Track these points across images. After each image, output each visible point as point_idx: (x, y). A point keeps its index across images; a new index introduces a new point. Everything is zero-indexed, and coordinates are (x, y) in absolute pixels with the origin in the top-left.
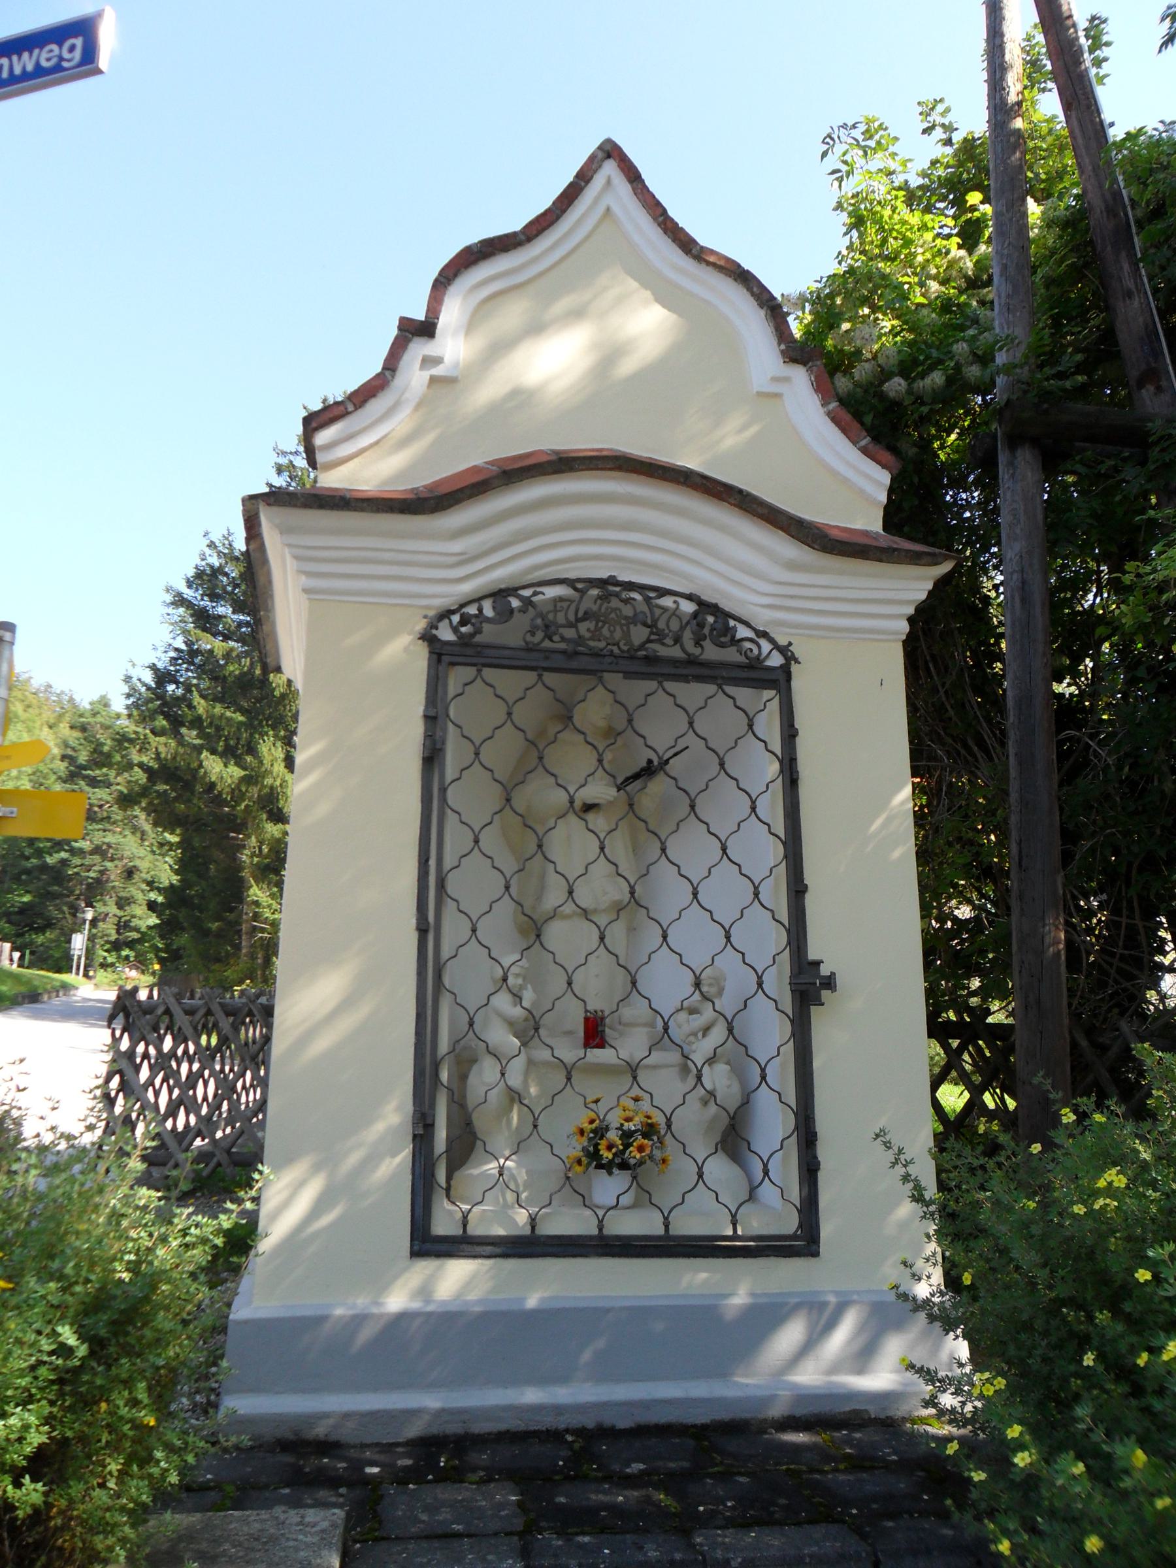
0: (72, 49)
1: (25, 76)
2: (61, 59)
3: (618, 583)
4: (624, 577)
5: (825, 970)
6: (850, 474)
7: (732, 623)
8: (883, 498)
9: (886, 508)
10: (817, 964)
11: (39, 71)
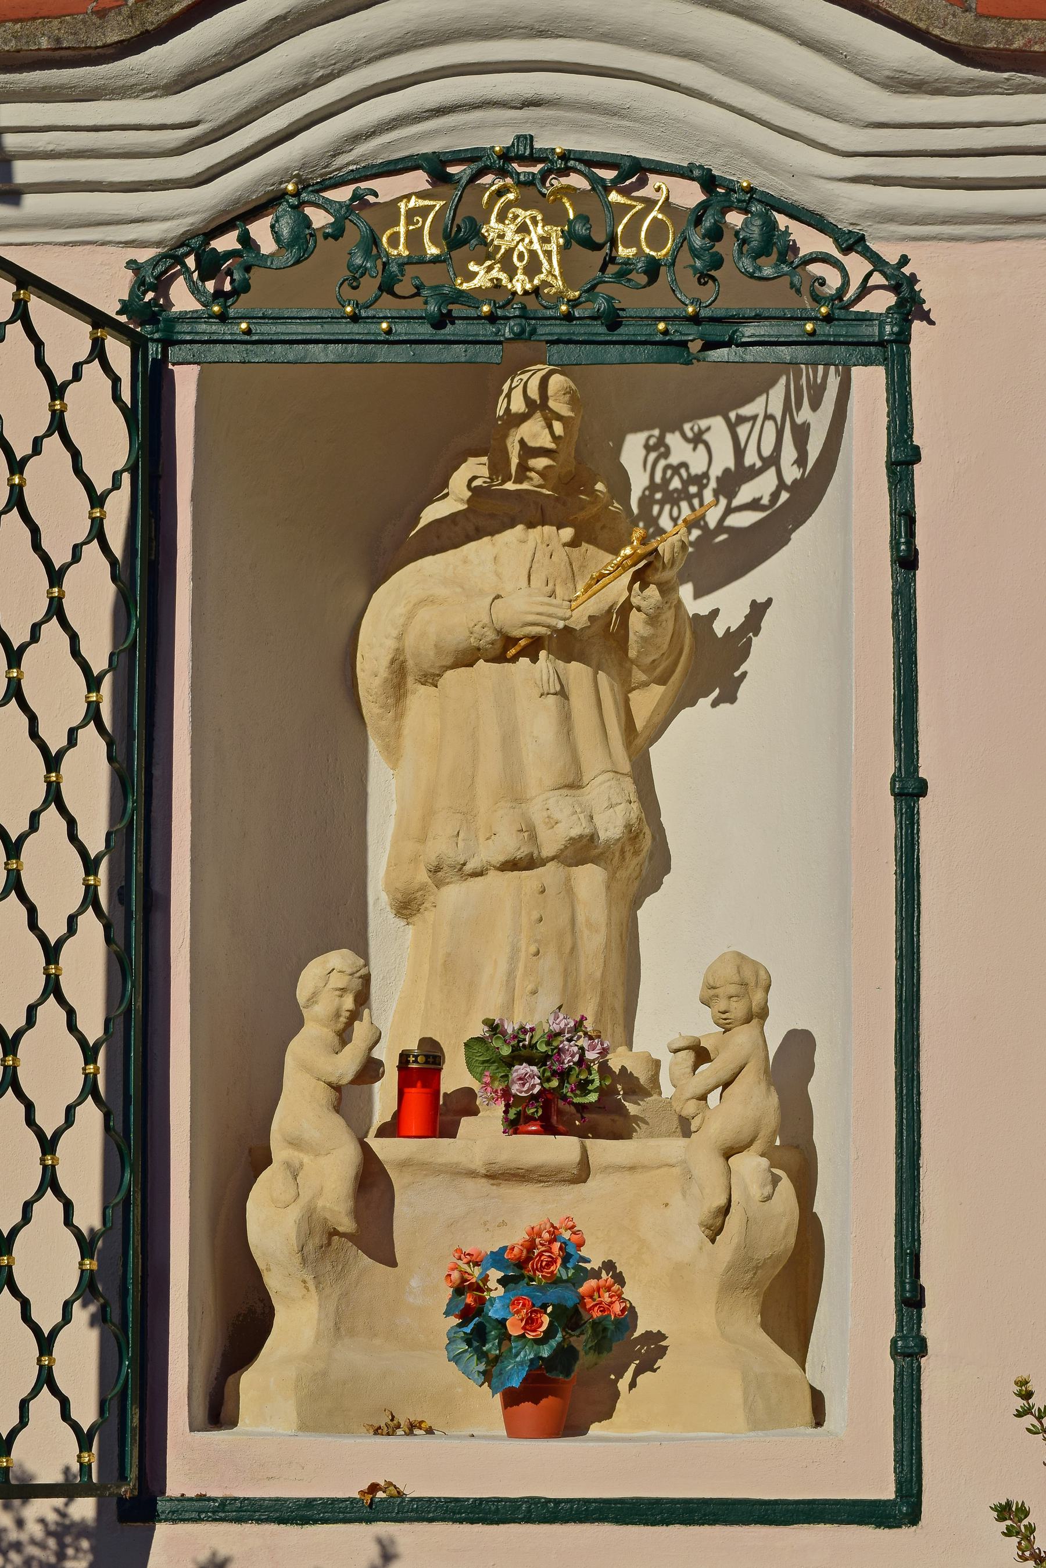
7: (782, 221)
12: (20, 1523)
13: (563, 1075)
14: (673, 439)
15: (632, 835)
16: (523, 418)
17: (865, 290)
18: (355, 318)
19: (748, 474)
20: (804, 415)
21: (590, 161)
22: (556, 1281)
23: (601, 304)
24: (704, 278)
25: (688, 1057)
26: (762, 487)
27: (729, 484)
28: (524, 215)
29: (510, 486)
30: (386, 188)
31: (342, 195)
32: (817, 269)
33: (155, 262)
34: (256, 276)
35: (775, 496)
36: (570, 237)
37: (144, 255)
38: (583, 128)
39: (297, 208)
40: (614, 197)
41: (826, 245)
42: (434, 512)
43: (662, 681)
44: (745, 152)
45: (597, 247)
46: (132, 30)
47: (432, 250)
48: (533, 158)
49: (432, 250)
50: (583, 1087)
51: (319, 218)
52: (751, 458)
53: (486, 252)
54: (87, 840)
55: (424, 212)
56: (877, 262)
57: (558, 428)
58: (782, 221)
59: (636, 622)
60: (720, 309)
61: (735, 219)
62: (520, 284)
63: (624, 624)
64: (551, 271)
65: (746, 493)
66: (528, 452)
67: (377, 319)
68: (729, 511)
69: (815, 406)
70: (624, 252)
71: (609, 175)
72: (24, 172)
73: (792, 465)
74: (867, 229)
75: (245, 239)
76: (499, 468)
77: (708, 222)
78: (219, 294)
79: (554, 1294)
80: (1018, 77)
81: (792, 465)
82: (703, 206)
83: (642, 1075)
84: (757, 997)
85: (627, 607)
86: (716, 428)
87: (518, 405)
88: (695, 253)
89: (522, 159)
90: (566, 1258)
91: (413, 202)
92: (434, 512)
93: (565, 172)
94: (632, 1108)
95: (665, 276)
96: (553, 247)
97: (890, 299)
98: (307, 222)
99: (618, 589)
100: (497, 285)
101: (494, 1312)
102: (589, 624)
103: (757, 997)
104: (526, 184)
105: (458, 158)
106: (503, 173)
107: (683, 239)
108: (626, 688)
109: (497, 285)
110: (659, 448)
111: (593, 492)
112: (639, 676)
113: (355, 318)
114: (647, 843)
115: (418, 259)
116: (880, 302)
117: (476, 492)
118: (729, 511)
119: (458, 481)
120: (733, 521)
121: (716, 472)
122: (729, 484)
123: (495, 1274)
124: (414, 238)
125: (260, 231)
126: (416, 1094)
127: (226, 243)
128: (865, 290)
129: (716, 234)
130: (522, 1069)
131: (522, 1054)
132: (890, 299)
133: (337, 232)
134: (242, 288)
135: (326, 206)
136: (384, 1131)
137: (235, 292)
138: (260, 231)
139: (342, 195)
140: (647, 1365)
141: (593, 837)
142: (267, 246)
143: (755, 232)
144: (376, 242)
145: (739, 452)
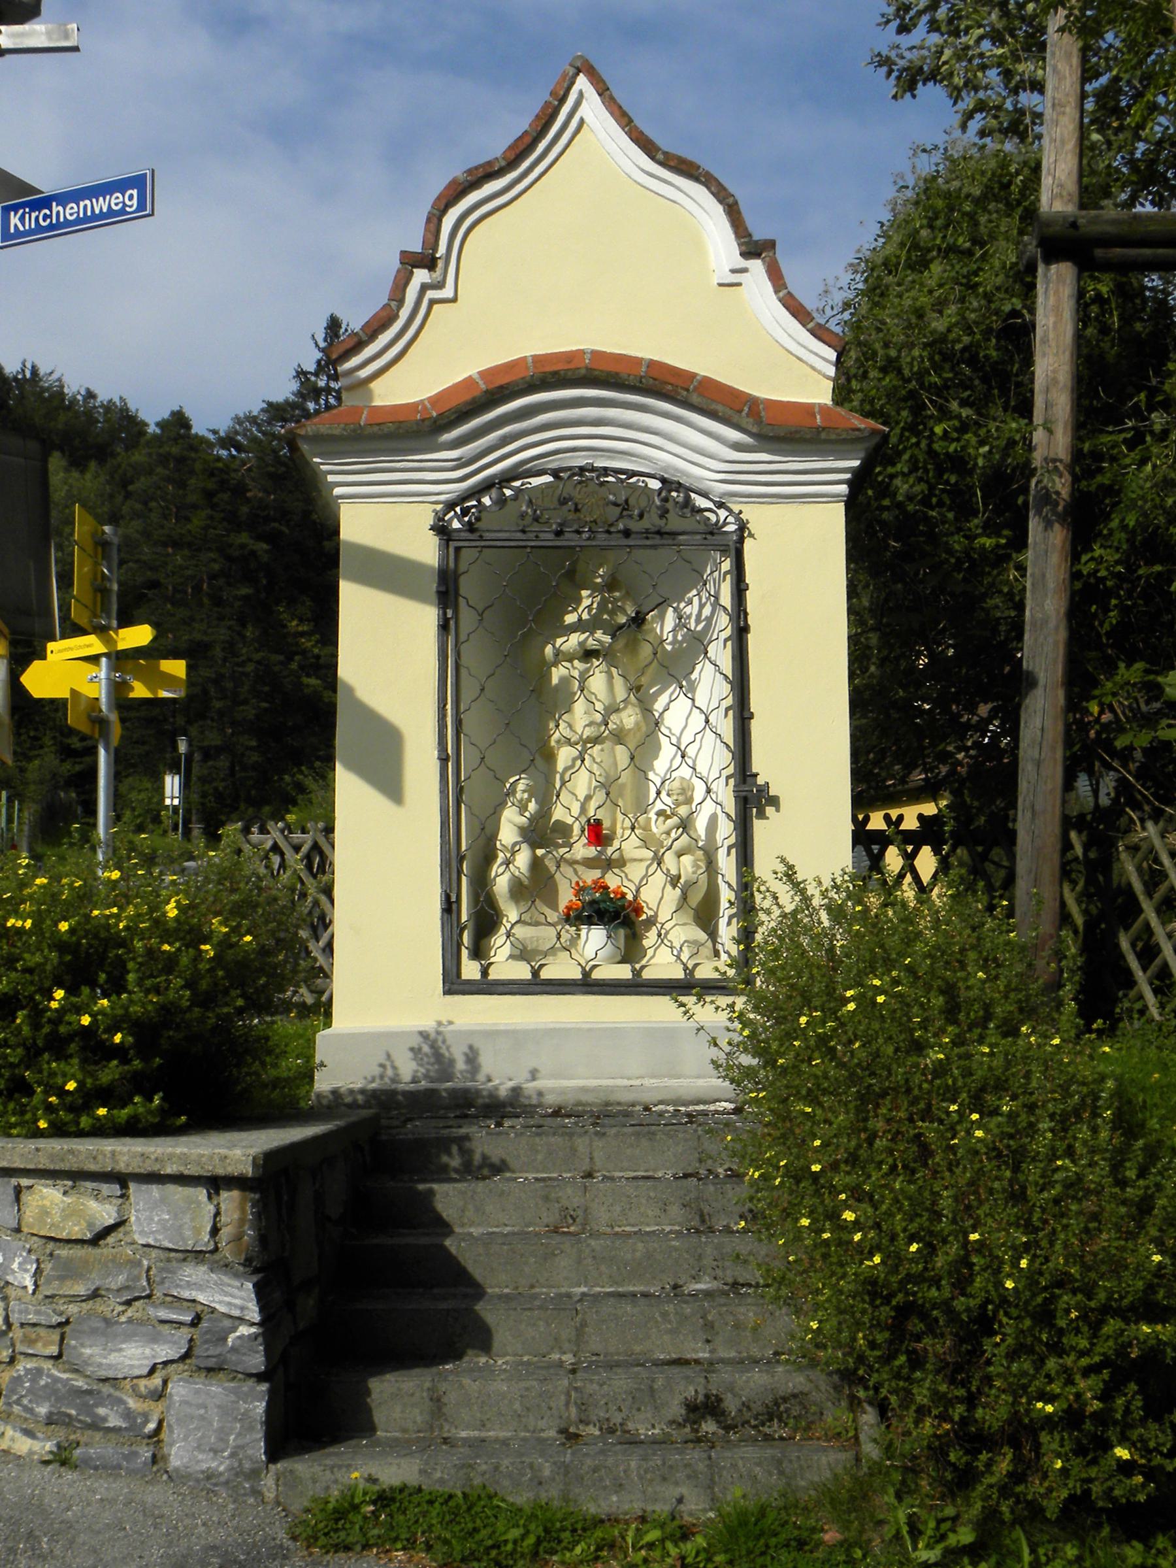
0: (131, 198)
1: (102, 216)
2: (125, 205)
3: (593, 469)
4: (600, 463)
5: (760, 781)
6: (801, 352)
7: (693, 495)
8: (831, 371)
9: (835, 380)
10: (756, 775)
11: (111, 213)
24: (662, 516)
32: (707, 514)
41: (710, 505)
51: (508, 492)
54: (16, 1158)
58: (693, 495)
60: (668, 529)
73: (783, 860)
81: (783, 860)
82: (661, 490)
102: (622, 932)
133: (515, 498)
139: (517, 484)
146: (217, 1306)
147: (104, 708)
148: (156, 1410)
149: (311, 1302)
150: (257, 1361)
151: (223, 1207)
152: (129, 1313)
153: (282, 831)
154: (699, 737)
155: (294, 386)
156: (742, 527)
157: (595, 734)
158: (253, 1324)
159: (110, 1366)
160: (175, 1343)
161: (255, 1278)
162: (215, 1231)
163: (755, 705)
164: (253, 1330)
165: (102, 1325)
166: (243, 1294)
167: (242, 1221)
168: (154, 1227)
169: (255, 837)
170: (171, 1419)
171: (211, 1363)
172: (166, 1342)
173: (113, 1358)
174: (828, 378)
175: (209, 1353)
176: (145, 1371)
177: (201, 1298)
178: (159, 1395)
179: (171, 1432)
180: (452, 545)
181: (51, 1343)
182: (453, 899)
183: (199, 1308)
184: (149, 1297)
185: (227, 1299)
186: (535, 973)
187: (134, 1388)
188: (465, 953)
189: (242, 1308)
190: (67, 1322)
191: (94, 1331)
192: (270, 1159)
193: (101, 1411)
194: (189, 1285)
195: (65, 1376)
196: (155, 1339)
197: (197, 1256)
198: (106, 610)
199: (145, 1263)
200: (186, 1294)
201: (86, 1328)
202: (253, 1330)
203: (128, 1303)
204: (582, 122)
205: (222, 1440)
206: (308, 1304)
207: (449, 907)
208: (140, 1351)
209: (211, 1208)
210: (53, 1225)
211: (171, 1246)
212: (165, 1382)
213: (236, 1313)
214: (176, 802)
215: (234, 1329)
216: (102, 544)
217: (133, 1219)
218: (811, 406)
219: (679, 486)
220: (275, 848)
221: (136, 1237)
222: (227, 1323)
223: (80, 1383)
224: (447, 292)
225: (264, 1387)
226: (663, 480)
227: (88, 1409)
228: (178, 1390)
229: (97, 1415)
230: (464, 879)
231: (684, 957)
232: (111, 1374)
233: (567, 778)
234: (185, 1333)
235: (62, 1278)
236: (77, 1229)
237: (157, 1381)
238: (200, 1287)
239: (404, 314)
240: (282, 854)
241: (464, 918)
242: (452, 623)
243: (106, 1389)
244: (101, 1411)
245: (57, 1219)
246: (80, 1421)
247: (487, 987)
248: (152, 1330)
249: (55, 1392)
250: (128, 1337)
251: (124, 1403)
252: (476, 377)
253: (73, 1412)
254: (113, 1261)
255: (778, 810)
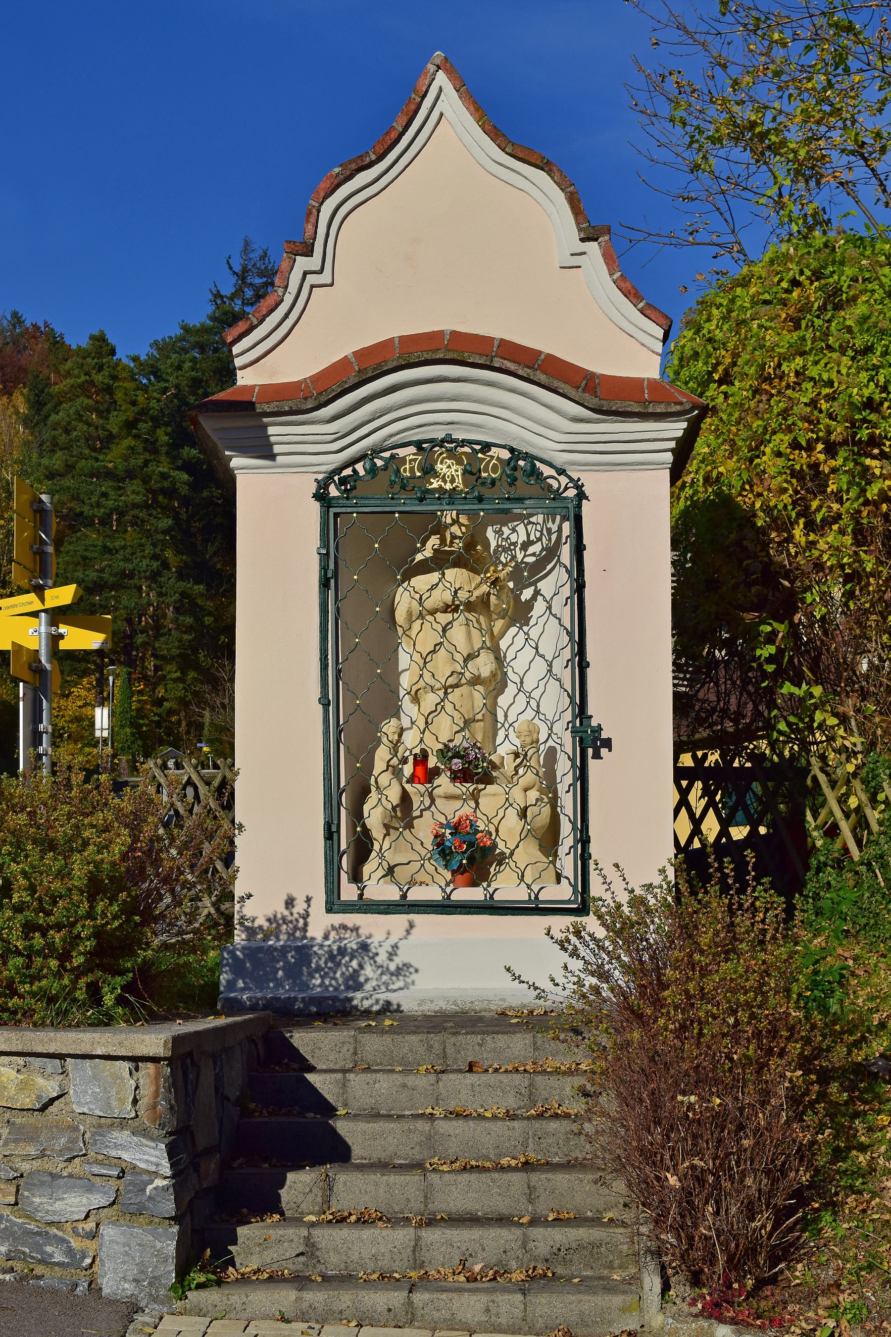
7: (538, 464)
8: (659, 347)
10: (591, 717)
12: (292, 914)
13: (470, 763)
14: (505, 529)
15: (493, 675)
16: (452, 525)
17: (566, 488)
18: (392, 498)
19: (532, 543)
20: (550, 525)
21: (470, 442)
22: (468, 833)
23: (476, 494)
24: (511, 484)
25: (512, 756)
26: (536, 548)
27: (525, 546)
28: (449, 462)
29: (447, 548)
30: (401, 452)
31: (387, 455)
33: (324, 479)
34: (358, 484)
35: (541, 552)
36: (465, 472)
37: (320, 477)
38: (469, 431)
39: (372, 459)
40: (480, 455)
41: (553, 472)
42: (419, 557)
43: (503, 618)
44: (524, 441)
45: (474, 474)
46: (316, 404)
47: (418, 474)
48: (452, 442)
49: (418, 474)
50: (477, 767)
51: (379, 463)
52: (532, 538)
53: (436, 475)
55: (415, 460)
56: (569, 477)
57: (463, 529)
58: (538, 464)
59: (493, 598)
61: (521, 463)
62: (448, 486)
63: (489, 599)
64: (459, 483)
65: (531, 550)
66: (454, 537)
67: (400, 499)
68: (525, 556)
69: (553, 523)
70: (484, 475)
71: (478, 447)
72: (277, 449)
74: (566, 467)
75: (354, 471)
76: (443, 541)
77: (512, 464)
78: (346, 490)
79: (467, 838)
80: (615, 418)
82: (510, 459)
83: (498, 762)
84: (535, 736)
85: (489, 594)
86: (521, 528)
87: (449, 521)
88: (508, 476)
89: (448, 442)
90: (471, 826)
91: (412, 457)
92: (419, 557)
93: (463, 446)
94: (494, 774)
95: (498, 483)
96: (459, 473)
97: (575, 492)
98: (375, 464)
99: (485, 588)
100: (441, 486)
101: (448, 844)
103: (535, 736)
104: (449, 451)
105: (426, 441)
106: (441, 447)
107: (504, 471)
108: (490, 620)
109: (441, 486)
110: (499, 533)
111: (475, 550)
112: (494, 616)
113: (392, 498)
114: (499, 677)
115: (413, 477)
116: (572, 493)
117: (435, 550)
118: (525, 556)
119: (429, 544)
120: (527, 560)
121: (520, 541)
122: (525, 546)
123: (448, 831)
124: (412, 470)
125: (359, 467)
126: (420, 769)
127: (348, 472)
128: (566, 488)
129: (515, 468)
130: (455, 760)
131: (457, 755)
132: (575, 492)
133: (385, 468)
134: (353, 488)
135: (382, 458)
136: (408, 782)
137: (351, 490)
138: (359, 467)
139: (387, 455)
140: (500, 864)
141: (479, 676)
142: (362, 473)
143: (528, 468)
144: (399, 471)
145: (528, 535)
146: (138, 1163)
147: (43, 660)
148: (91, 1246)
149: (213, 1166)
150: (169, 1207)
151: (141, 1081)
152: (70, 1170)
153: (195, 768)
154: (542, 683)
155: (210, 309)
156: (581, 496)
157: (455, 682)
158: (166, 1177)
159: (54, 1213)
160: (105, 1193)
161: (167, 1141)
162: (135, 1101)
163: (589, 657)
164: (165, 1182)
165: (49, 1179)
166: (157, 1153)
167: (156, 1093)
168: (88, 1098)
169: (172, 772)
170: (103, 1255)
171: (133, 1209)
172: (99, 1192)
173: (58, 1205)
174: (657, 354)
175: (132, 1201)
176: (83, 1217)
177: (125, 1156)
178: (93, 1235)
179: (103, 1265)
180: (332, 511)
181: (10, 1194)
182: (334, 829)
183: (124, 1165)
184: (85, 1155)
185: (146, 1157)
186: (404, 896)
187: (75, 1230)
188: (344, 877)
189: (157, 1165)
190: (22, 1176)
191: (42, 1183)
192: (177, 1041)
193: (49, 1249)
194: (116, 1146)
195: (20, 1221)
196: (90, 1189)
197: (122, 1123)
198: (44, 574)
199: (82, 1127)
200: (113, 1153)
201: (36, 1181)
202: (165, 1182)
203: (70, 1160)
204: (442, 115)
205: (142, 1272)
206: (212, 1166)
207: (331, 834)
208: (78, 1199)
209: (133, 1083)
210: (10, 1097)
211: (102, 1114)
212: (98, 1225)
213: (153, 1168)
214: (105, 734)
215: (152, 1182)
216: (39, 511)
217: (71, 1092)
218: (640, 381)
219: (527, 456)
220: (190, 782)
221: (74, 1107)
222: (145, 1177)
223: (32, 1226)
224: (325, 278)
225: (175, 1229)
226: (512, 450)
227: (39, 1248)
228: (108, 1232)
229: (44, 1252)
230: (343, 812)
231: (528, 879)
232: (56, 1219)
233: (430, 721)
234: (114, 1183)
235: (16, 1141)
236: (28, 1101)
237: (90, 1225)
238: (123, 1147)
239: (288, 299)
240: (196, 789)
241: (343, 846)
242: (332, 581)
243: (54, 1231)
244: (49, 1249)
245: (13, 1092)
246: (33, 1258)
247: (365, 906)
248: (87, 1184)
249: (13, 1233)
250: (69, 1189)
251: (68, 1242)
252: (351, 357)
253: (27, 1250)
254: (57, 1127)
255: (610, 750)
